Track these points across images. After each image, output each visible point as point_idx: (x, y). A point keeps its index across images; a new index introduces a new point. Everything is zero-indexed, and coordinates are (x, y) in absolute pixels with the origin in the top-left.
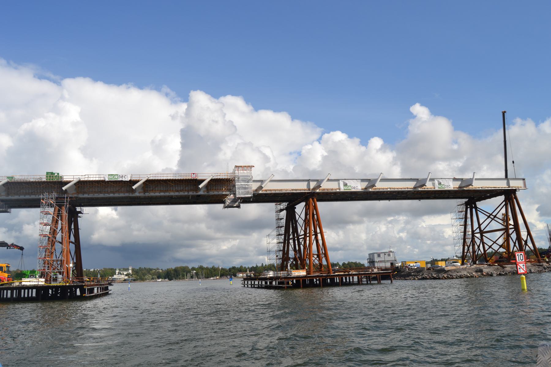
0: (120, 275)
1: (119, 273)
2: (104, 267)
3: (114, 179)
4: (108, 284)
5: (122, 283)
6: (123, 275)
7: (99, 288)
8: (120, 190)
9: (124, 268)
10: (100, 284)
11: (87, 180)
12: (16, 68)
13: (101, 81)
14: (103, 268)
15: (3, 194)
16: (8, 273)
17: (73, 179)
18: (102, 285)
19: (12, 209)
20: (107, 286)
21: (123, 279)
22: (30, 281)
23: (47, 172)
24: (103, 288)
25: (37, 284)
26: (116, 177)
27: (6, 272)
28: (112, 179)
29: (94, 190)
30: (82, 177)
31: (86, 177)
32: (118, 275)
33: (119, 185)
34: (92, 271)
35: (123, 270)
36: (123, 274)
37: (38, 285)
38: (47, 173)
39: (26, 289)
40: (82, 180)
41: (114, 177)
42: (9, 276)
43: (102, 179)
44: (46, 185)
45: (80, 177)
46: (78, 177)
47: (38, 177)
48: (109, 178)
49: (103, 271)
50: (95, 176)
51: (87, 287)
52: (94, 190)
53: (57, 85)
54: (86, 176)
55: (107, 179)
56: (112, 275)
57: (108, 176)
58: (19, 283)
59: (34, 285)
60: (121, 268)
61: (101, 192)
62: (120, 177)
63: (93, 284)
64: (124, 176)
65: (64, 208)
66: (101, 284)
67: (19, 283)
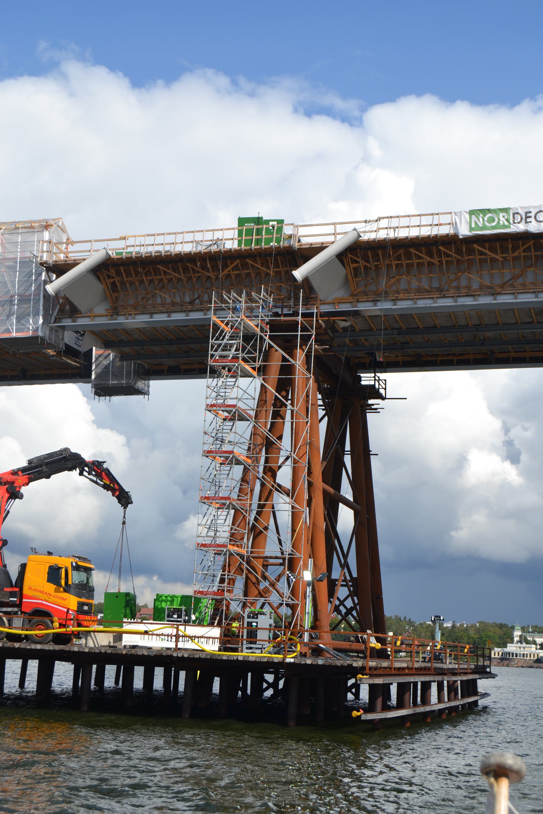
0: (524, 645)
1: (523, 640)
2: (481, 620)
3: (493, 228)
4: (474, 672)
5: (530, 667)
6: (534, 646)
7: (434, 688)
8: (520, 280)
9: (536, 627)
10: (436, 669)
11: (385, 240)
12: (252, 95)
13: (463, 100)
14: (480, 622)
15: (101, 309)
16: (79, 596)
17: (331, 239)
18: (445, 674)
19: (152, 383)
20: (471, 677)
21: (532, 658)
22: (146, 633)
23: (242, 216)
24: (452, 688)
25: (172, 645)
26: (503, 221)
27: (72, 590)
28: (484, 228)
29: (415, 284)
30: (367, 229)
31: (381, 226)
32: (519, 645)
33: (516, 254)
34: (447, 627)
35: (533, 632)
36: (534, 643)
37: (177, 649)
38: (242, 221)
39: (139, 665)
40: (365, 237)
41: (492, 220)
42: (86, 608)
43: (444, 230)
44: (236, 268)
45: (360, 227)
46: (350, 227)
47: (209, 236)
48: (473, 226)
49: (478, 630)
50: (415, 221)
51: (372, 676)
52: (415, 284)
53: (351, 125)
54: (384, 223)
55: (464, 231)
56: (501, 642)
57: (467, 216)
58: (111, 635)
59: (134, 647)
60: (529, 626)
61: (442, 292)
62: (518, 218)
63: (404, 665)
64: (532, 215)
65: (300, 355)
66: (442, 669)
67: (111, 635)
